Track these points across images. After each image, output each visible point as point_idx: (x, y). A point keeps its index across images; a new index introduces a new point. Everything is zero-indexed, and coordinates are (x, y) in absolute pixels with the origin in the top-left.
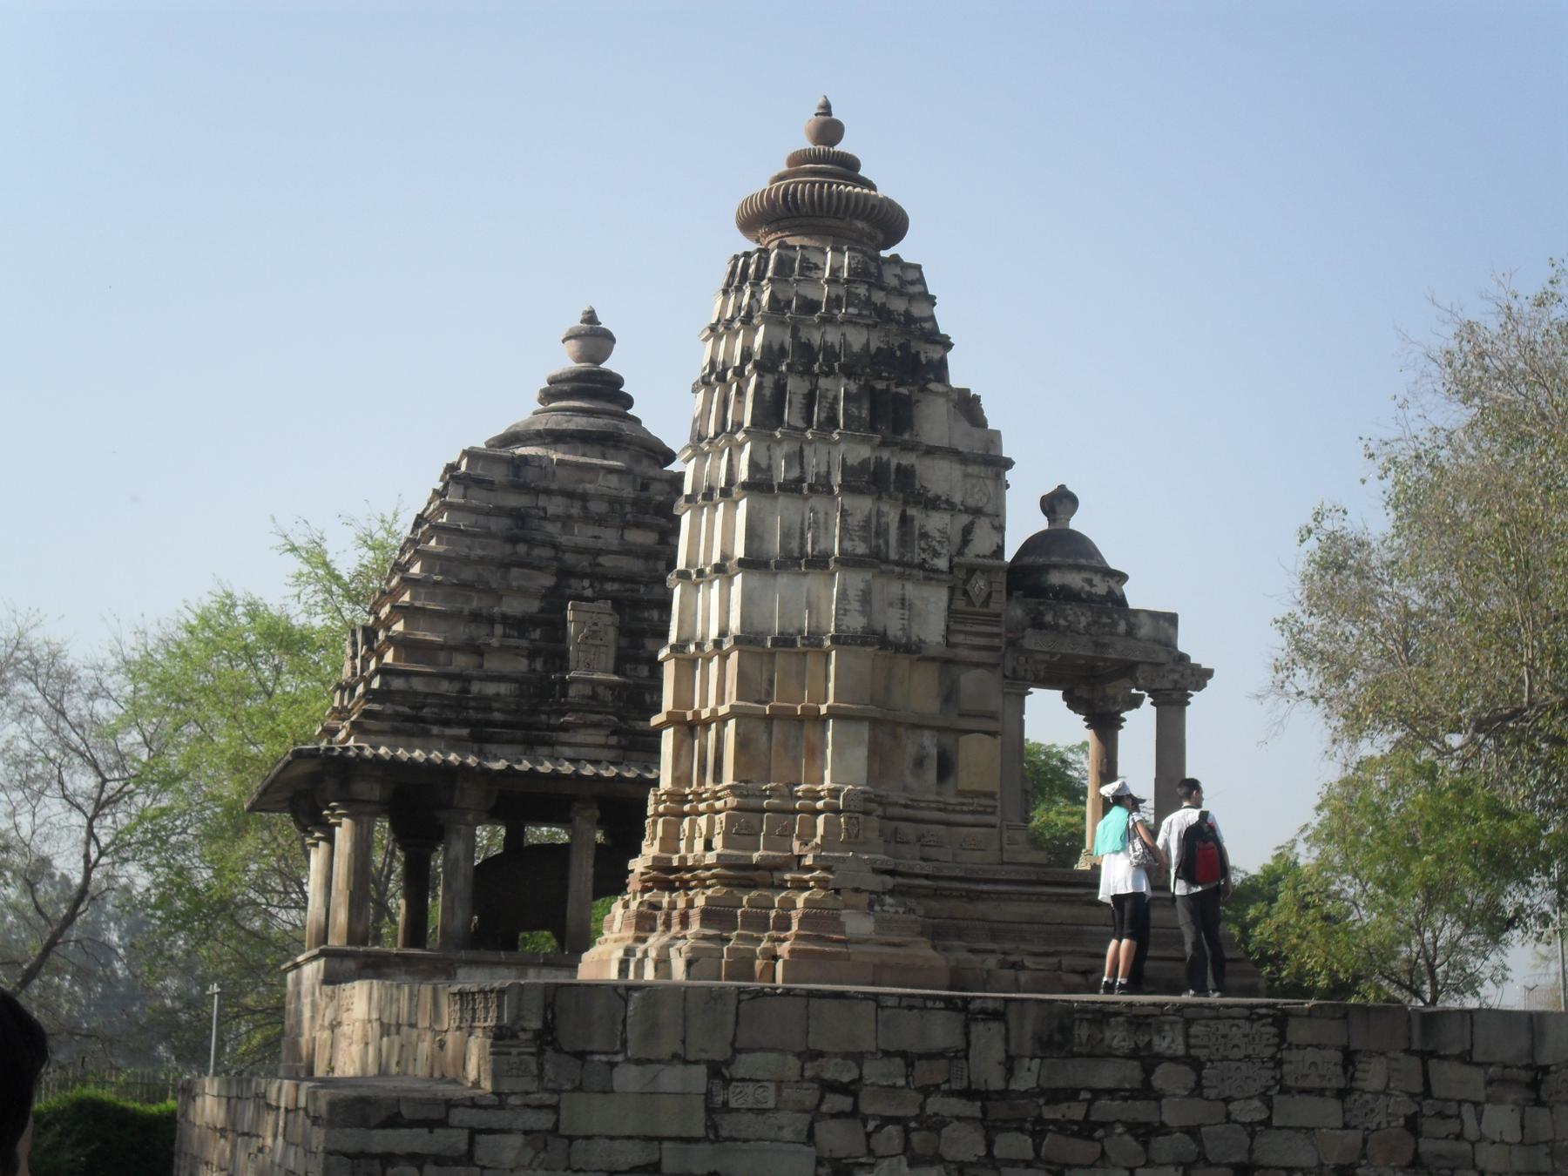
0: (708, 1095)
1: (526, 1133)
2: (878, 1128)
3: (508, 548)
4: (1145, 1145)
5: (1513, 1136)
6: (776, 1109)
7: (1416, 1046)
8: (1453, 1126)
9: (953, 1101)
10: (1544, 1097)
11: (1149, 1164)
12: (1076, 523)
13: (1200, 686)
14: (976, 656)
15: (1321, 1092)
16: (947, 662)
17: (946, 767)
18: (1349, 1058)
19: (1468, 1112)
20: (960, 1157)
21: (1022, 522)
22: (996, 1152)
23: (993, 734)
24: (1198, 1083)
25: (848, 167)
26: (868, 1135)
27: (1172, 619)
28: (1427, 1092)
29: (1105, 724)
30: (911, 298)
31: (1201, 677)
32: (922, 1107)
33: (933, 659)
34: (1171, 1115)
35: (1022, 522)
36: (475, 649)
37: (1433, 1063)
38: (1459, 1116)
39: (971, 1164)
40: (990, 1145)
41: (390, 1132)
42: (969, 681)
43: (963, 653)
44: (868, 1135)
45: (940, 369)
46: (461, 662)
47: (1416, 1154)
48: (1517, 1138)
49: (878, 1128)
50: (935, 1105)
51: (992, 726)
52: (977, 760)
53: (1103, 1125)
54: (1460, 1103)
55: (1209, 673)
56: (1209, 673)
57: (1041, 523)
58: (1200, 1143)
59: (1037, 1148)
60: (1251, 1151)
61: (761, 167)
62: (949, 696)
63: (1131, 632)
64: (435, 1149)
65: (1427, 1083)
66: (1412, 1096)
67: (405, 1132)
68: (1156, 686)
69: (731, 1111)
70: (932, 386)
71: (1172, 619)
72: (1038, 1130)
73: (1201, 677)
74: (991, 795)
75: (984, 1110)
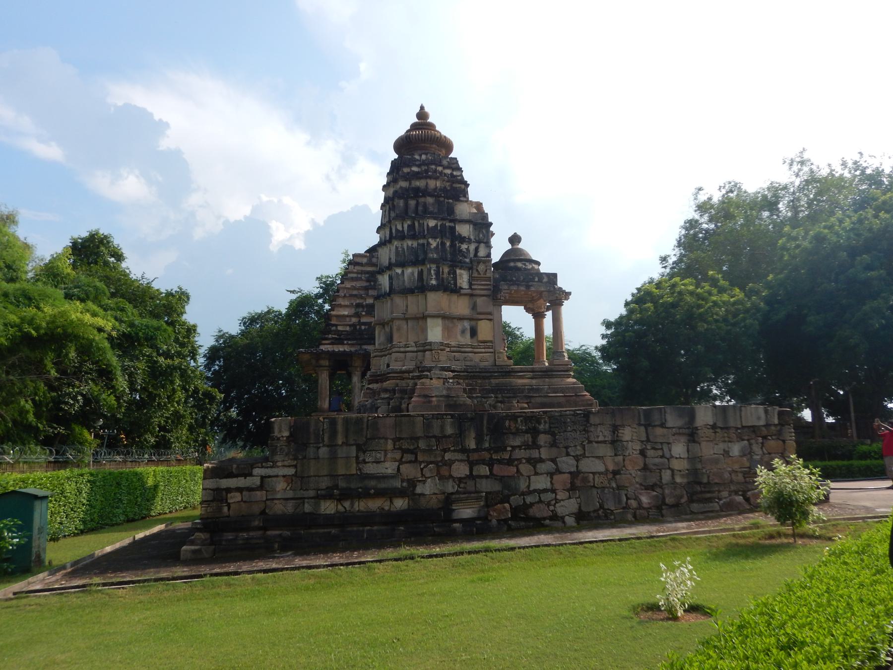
0: (357, 457)
1: (284, 476)
2: (425, 467)
3: (368, 284)
4: (535, 467)
5: (685, 455)
6: (384, 461)
7: (643, 422)
8: (660, 453)
9: (456, 454)
10: (696, 439)
11: (536, 474)
12: (521, 246)
13: (567, 299)
14: (483, 292)
15: (604, 442)
16: (471, 295)
17: (474, 333)
18: (615, 429)
19: (665, 447)
20: (459, 476)
21: (499, 249)
22: (474, 473)
23: (490, 320)
24: (554, 440)
25: (432, 126)
26: (422, 469)
27: (555, 275)
28: (648, 440)
29: (538, 317)
30: (453, 169)
31: (567, 295)
32: (443, 457)
33: (465, 295)
34: (544, 453)
35: (499, 249)
36: (357, 315)
37: (650, 429)
38: (662, 449)
39: (464, 478)
40: (471, 470)
41: (230, 480)
42: (480, 301)
43: (478, 292)
44: (422, 469)
45: (465, 194)
46: (354, 320)
47: (645, 464)
48: (686, 456)
49: (425, 467)
50: (448, 456)
51: (490, 317)
52: (485, 330)
53: (517, 459)
54: (662, 443)
55: (570, 293)
56: (570, 293)
57: (509, 247)
58: (556, 464)
59: (491, 470)
60: (577, 467)
61: (401, 128)
62: (474, 307)
63: (540, 281)
64: (247, 485)
65: (648, 437)
66: (642, 442)
67: (235, 479)
68: (551, 299)
69: (366, 463)
70: (462, 199)
71: (555, 275)
72: (491, 464)
73: (567, 295)
74: (491, 342)
75: (468, 457)
